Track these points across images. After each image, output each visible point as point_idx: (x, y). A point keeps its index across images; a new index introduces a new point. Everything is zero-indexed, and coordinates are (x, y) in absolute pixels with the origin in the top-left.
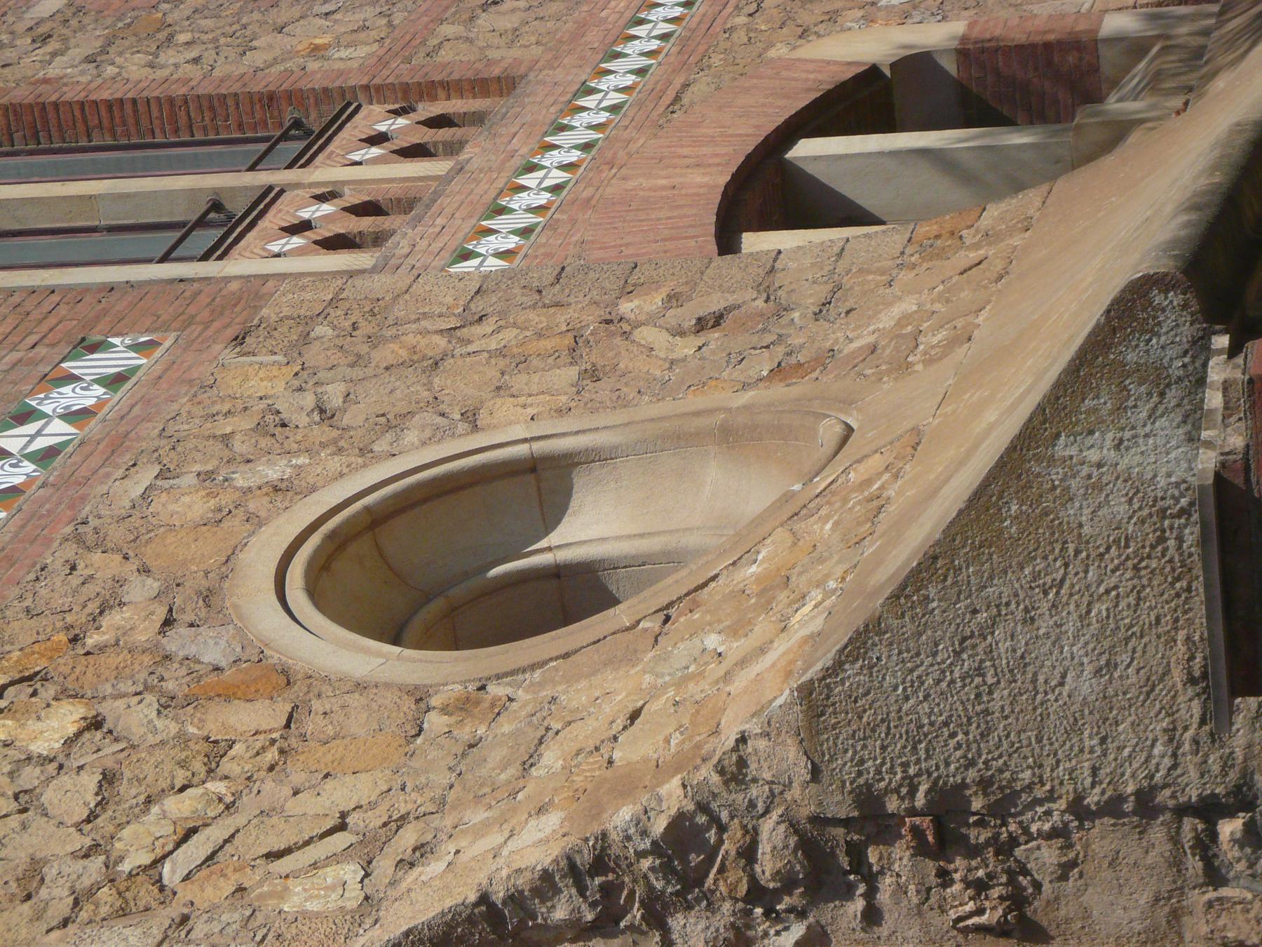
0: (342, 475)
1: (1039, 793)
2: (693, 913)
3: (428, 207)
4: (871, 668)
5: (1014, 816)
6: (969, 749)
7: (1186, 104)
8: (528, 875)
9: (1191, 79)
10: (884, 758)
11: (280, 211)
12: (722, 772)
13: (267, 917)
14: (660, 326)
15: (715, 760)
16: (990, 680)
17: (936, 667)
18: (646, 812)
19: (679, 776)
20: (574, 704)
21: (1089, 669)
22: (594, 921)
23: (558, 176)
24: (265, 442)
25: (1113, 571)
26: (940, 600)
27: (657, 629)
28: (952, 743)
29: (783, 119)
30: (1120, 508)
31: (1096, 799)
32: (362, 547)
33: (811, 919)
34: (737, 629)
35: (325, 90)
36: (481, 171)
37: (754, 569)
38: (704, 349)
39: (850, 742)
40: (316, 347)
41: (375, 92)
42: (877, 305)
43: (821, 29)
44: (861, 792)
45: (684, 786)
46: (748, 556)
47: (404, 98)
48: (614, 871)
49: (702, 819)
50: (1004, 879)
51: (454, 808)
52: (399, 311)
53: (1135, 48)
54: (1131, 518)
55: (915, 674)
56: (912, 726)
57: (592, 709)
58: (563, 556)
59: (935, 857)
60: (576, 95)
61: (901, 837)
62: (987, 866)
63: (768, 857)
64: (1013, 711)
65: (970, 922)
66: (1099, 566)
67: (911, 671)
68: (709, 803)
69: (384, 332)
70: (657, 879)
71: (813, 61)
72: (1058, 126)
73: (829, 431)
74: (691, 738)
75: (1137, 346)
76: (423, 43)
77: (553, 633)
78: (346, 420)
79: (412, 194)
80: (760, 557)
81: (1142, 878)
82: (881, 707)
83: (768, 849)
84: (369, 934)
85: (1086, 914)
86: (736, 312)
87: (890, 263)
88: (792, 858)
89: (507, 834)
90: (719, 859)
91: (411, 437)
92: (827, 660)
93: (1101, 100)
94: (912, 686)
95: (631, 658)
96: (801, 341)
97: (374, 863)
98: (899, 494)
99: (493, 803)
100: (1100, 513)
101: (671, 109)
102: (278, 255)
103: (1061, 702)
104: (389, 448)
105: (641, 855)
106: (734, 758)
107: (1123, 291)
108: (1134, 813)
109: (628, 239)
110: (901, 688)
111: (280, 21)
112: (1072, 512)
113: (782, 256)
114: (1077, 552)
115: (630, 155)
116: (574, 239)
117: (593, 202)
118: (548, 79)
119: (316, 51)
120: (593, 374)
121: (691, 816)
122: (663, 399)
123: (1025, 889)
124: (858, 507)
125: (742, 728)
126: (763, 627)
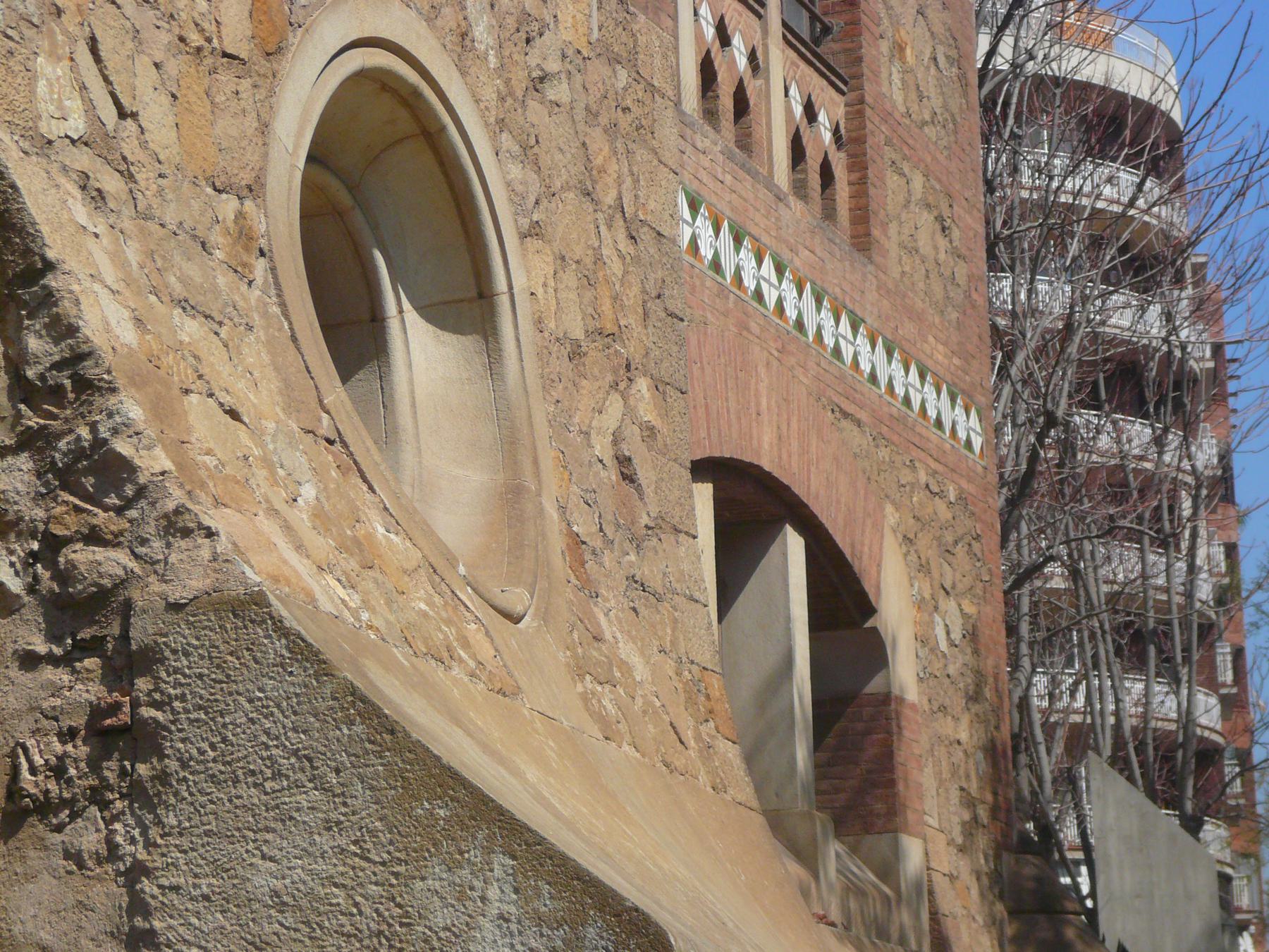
0: (477, 101)
1: (154, 833)
2: (34, 478)
3: (743, 167)
4: (282, 665)
5: (131, 807)
6: (198, 762)
7: (833, 924)
8: (74, 312)
9: (858, 929)
10: (190, 677)
11: (741, 15)
12: (177, 512)
13: (31, 40)
14: (623, 420)
15: (190, 505)
16: (268, 785)
17: (282, 731)
18: (137, 434)
19: (173, 468)
20: (246, 350)
21: (278, 884)
22: (26, 378)
23: (771, 297)
24: (511, 22)
25: (377, 911)
26: (349, 736)
27: (321, 432)
28: (205, 746)
29: (824, 521)
30: (441, 918)
31: (147, 889)
32: (405, 123)
33: (26, 599)
34: (320, 516)
35: (859, 60)
36: (778, 219)
37: (381, 530)
38: (600, 466)
39: (207, 643)
40: (606, 71)
41: (857, 110)
42: (642, 639)
43: (913, 557)
44: (156, 653)
45: (163, 473)
46: (394, 524)
47: (850, 139)
48: (76, 399)
49: (129, 490)
50: (66, 795)
51: (142, 230)
52: (641, 154)
53: (888, 870)
54: (430, 929)
55: (275, 710)
56: (223, 706)
57: (240, 369)
58: (394, 325)
59: (89, 725)
60: (851, 313)
61: (110, 692)
62: (79, 778)
63: (91, 557)
64: (236, 807)
65: (23, 760)
66: (382, 897)
67: (278, 706)
68: (146, 498)
69: (620, 140)
70: (68, 443)
71: (881, 549)
72: (813, 791)
73: (517, 598)
74: (211, 476)
75: (602, 938)
76: (905, 158)
77: (317, 324)
78: (533, 104)
79: (755, 148)
80: (392, 536)
81: (66, 934)
82: (242, 674)
83: (99, 557)
84: (14, 146)
85: (31, 877)
86: (636, 496)
87: (683, 651)
88: (89, 581)
89: (114, 287)
90: (89, 507)
91: (515, 171)
92: (290, 622)
93: (838, 835)
94: (263, 707)
95: (292, 406)
96: (607, 564)
97: (86, 148)
98: (453, 680)
99: (146, 271)
100: (435, 898)
101: (836, 409)
102: (696, 13)
103: (245, 855)
104: (504, 149)
105: (93, 427)
106: (191, 525)
107: (657, 925)
108: (133, 928)
109: (708, 370)
110: (261, 695)
111: (930, 13)
112: (437, 870)
113: (691, 540)
114: (396, 875)
115: (791, 369)
116: (709, 315)
117: (745, 333)
118: (867, 284)
119: (899, 48)
120: (576, 354)
121: (133, 481)
122: (551, 426)
123: (56, 816)
124: (441, 637)
125: (222, 533)
126: (322, 545)
